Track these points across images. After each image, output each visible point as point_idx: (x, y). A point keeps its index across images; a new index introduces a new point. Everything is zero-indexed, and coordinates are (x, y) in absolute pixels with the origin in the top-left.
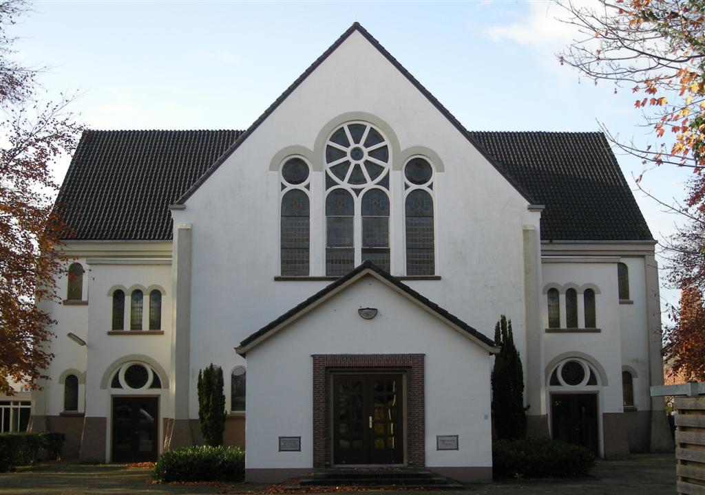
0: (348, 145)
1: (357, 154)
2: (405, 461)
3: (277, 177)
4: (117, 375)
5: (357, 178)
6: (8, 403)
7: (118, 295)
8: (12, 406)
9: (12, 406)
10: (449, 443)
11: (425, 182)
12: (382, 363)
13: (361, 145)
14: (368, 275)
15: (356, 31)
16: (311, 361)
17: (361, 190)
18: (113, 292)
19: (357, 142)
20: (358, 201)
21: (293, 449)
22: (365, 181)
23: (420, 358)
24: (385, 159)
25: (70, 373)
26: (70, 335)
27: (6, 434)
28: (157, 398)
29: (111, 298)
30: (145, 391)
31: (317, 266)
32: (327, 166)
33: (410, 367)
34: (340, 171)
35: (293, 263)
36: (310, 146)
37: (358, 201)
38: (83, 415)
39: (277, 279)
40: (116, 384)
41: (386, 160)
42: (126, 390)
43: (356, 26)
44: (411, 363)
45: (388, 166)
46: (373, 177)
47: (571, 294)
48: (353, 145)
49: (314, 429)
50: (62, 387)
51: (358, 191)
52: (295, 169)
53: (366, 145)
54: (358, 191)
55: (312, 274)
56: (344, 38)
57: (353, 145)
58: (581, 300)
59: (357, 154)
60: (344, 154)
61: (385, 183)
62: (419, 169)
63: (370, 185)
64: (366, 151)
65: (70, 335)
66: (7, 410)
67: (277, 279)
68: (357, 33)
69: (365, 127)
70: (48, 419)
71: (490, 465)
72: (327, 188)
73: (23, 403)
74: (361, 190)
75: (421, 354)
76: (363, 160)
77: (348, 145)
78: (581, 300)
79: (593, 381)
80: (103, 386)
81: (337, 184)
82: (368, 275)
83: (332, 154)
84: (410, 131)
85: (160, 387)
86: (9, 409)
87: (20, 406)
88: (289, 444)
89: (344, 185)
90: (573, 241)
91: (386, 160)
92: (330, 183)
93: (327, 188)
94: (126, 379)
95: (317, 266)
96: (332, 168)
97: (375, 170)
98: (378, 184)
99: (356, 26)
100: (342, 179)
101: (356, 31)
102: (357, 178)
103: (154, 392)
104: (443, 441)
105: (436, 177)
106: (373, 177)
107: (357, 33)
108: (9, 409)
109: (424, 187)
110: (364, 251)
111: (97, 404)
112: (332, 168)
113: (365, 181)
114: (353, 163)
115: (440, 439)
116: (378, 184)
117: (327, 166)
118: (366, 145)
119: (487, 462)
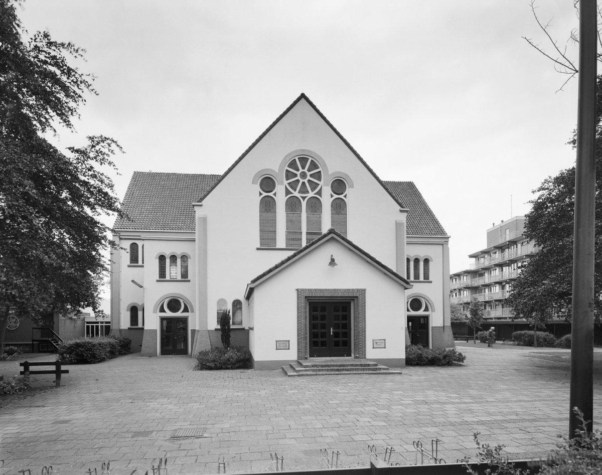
0: (298, 170)
1: (303, 175)
2: (353, 355)
3: (257, 188)
4: (163, 304)
5: (304, 190)
6: (98, 323)
7: (162, 258)
8: (99, 325)
9: (99, 325)
10: (380, 344)
11: (342, 194)
12: (340, 295)
13: (306, 170)
14: (332, 238)
15: (303, 99)
16: (296, 293)
17: (306, 197)
18: (158, 257)
19: (303, 168)
20: (304, 204)
21: (379, 346)
22: (308, 192)
23: (363, 291)
24: (320, 179)
25: (133, 305)
26: (133, 281)
27: (405, 243)
28: (187, 318)
29: (158, 260)
30: (179, 314)
31: (281, 242)
32: (286, 182)
33: (357, 297)
34: (293, 185)
35: (267, 242)
36: (276, 169)
37: (304, 204)
38: (143, 329)
39: (258, 249)
40: (162, 310)
41: (320, 180)
42: (169, 314)
43: (303, 96)
44: (358, 295)
45: (321, 183)
46: (312, 190)
47: (417, 261)
48: (301, 170)
49: (298, 336)
50: (128, 314)
51: (304, 198)
52: (267, 183)
53: (309, 171)
54: (304, 198)
55: (277, 247)
56: (295, 103)
57: (301, 170)
58: (422, 264)
59: (303, 175)
60: (296, 175)
61: (319, 193)
62: (339, 185)
63: (311, 194)
64: (308, 174)
65: (133, 281)
66: (97, 327)
67: (258, 249)
68: (303, 100)
69: (308, 159)
70: (121, 330)
71: (405, 357)
72: (286, 196)
73: (106, 323)
74: (306, 197)
75: (362, 290)
76: (304, 181)
77: (298, 170)
78: (422, 264)
79: (426, 309)
80: (155, 312)
81: (292, 193)
82: (332, 238)
83: (289, 175)
84: (334, 163)
85: (188, 312)
86: (98, 326)
87: (104, 324)
88: (282, 345)
89: (296, 194)
90: (247, 291)
91: (320, 180)
92: (288, 192)
93: (286, 196)
94: (168, 308)
95: (281, 242)
96: (289, 184)
97: (314, 186)
98: (315, 194)
99: (303, 96)
100: (295, 190)
101: (303, 99)
102: (304, 190)
103: (185, 314)
104: (377, 343)
105: (348, 191)
106: (312, 190)
107: (303, 100)
108: (98, 326)
109: (342, 196)
110: (308, 233)
111: (152, 322)
112: (289, 184)
113: (308, 192)
114: (301, 181)
115: (375, 341)
116: (315, 194)
117: (286, 182)
118: (309, 171)
119: (403, 356)
